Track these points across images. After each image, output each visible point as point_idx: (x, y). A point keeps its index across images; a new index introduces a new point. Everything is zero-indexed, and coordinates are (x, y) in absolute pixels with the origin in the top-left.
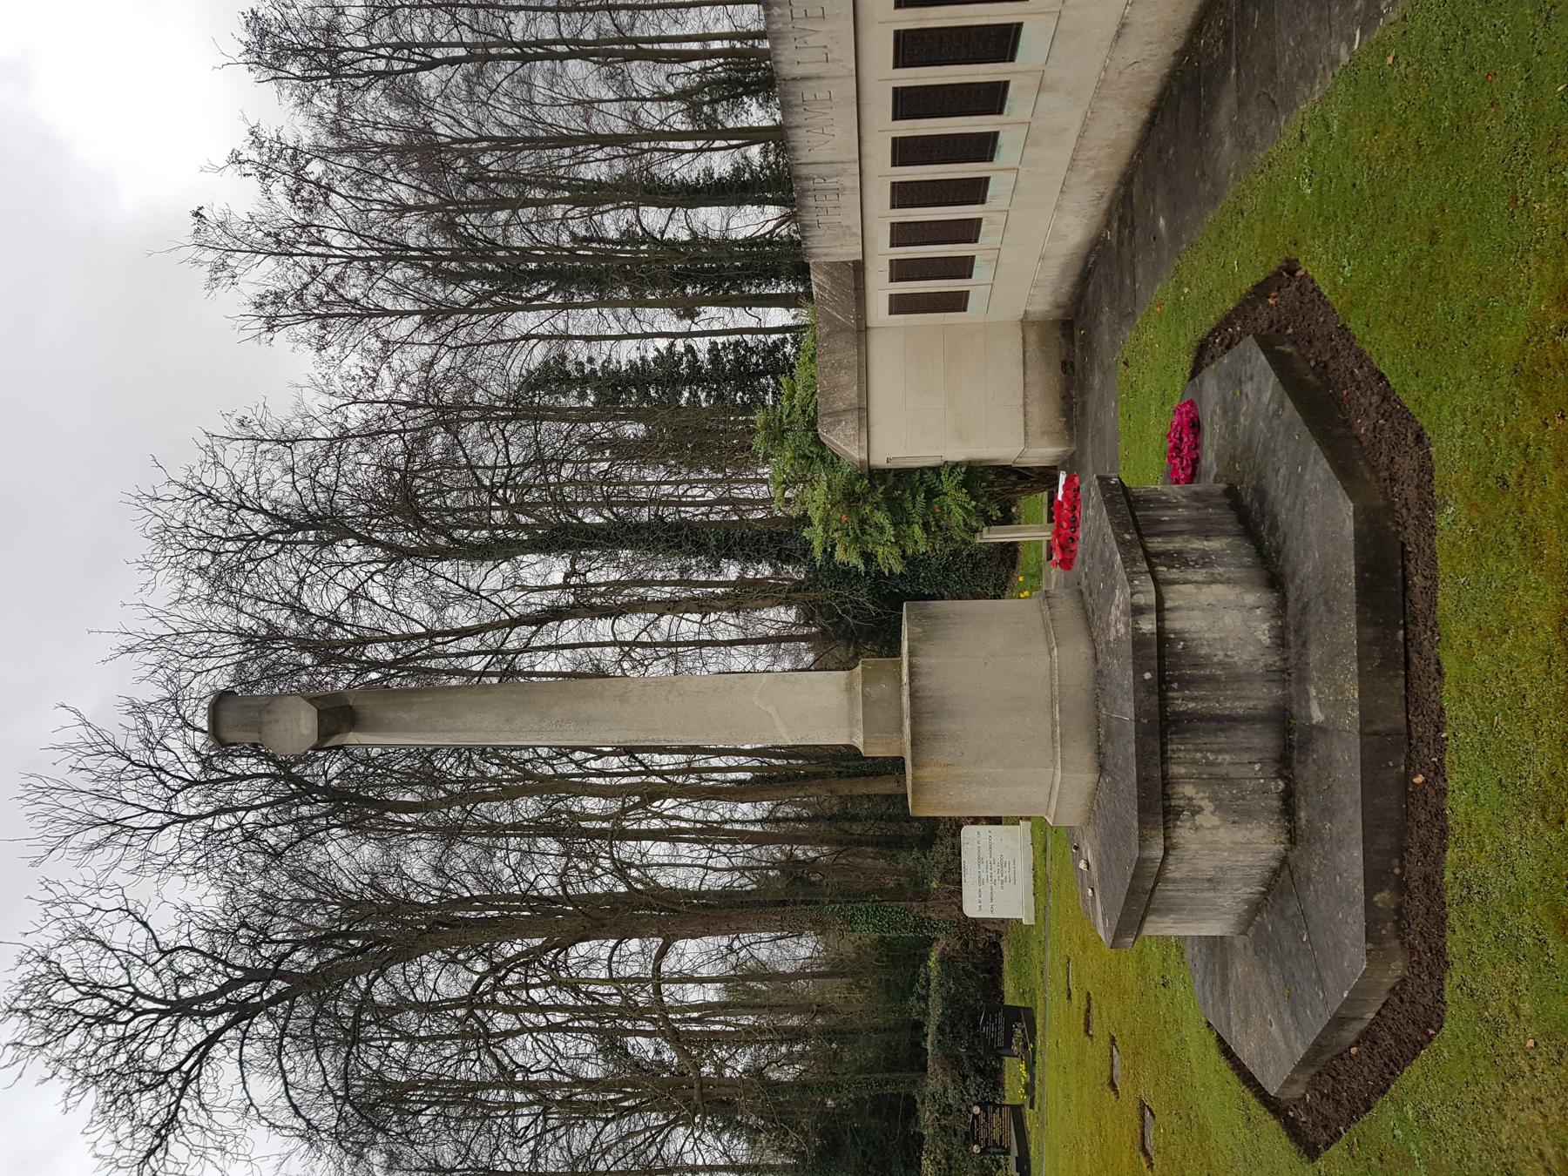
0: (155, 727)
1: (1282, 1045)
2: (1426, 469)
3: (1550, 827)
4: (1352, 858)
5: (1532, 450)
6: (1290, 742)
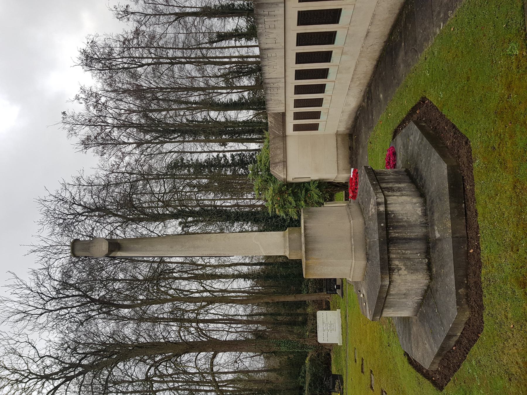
0: (41, 279)
1: (430, 350)
2: (469, 151)
3: (514, 253)
4: (451, 280)
5: (502, 136)
6: (429, 245)
